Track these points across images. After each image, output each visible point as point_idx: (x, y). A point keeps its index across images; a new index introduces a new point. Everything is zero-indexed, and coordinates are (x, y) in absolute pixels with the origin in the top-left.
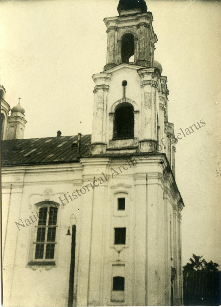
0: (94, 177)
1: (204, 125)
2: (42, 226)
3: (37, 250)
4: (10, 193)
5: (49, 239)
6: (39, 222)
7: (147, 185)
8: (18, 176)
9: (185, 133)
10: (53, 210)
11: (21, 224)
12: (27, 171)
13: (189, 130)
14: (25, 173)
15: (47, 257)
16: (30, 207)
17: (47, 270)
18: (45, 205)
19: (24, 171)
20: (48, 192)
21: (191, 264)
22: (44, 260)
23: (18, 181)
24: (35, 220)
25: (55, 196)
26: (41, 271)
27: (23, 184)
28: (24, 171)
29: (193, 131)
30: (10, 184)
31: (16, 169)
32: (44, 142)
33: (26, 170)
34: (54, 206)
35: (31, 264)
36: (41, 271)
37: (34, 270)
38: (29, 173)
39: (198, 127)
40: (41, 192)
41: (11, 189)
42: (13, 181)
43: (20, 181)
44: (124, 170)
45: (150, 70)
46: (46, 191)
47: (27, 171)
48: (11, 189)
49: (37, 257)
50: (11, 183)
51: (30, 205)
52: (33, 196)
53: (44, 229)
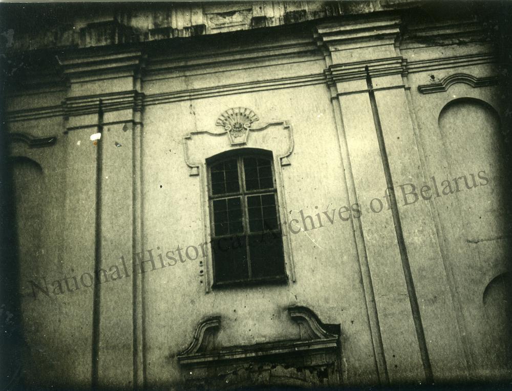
1: (170, 255)
9: (440, 190)
13: (449, 185)
39: (470, 183)
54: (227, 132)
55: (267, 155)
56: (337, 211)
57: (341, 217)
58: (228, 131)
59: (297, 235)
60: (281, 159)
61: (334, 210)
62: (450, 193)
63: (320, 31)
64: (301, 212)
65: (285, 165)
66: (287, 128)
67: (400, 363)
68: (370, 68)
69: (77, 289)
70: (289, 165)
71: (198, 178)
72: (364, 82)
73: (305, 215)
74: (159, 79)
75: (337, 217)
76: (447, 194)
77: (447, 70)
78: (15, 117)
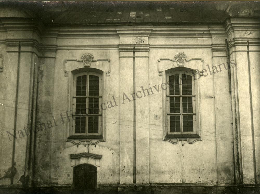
0: (134, 47)
2: (175, 96)
3: (171, 122)
4: (134, 58)
5: (184, 110)
6: (171, 91)
7: (134, 58)
8: (140, 38)
10: (94, 79)
11: (157, 89)
12: (152, 33)
14: (150, 34)
15: (185, 130)
16: (161, 74)
17: (190, 143)
18: (175, 73)
19: (150, 32)
20: (180, 58)
21: (67, 187)
22: (182, 132)
23: (142, 43)
24: (220, 71)
25: (190, 62)
26: (183, 145)
27: (148, 48)
28: (150, 32)
29: (221, 71)
30: (133, 46)
31: (140, 29)
32: (44, 160)
33: (152, 30)
34: (95, 74)
35: (168, 138)
36: (183, 145)
37: (174, 143)
38: (156, 34)
40: (172, 58)
41: (134, 52)
42: (135, 43)
43: (144, 43)
44: (208, 76)
45: (87, 128)
46: (50, 167)
47: (152, 33)
48: (134, 52)
49: (172, 130)
50: (134, 45)
51: (66, 72)
52: (162, 62)
53: (178, 99)
54: (83, 62)
55: (101, 72)
56: (160, 86)
57: (162, 88)
58: (83, 61)
59: (141, 99)
60: (106, 73)
61: (159, 85)
62: (217, 72)
63: (232, 22)
64: (142, 87)
65: (107, 76)
66: (109, 62)
67: (209, 168)
68: (135, 50)
69: (123, 104)
70: (109, 76)
71: (67, 77)
72: (132, 53)
73: (144, 89)
74: (70, 38)
75: (160, 88)
76: (110, 108)
77: (177, 50)
78: (60, 31)
